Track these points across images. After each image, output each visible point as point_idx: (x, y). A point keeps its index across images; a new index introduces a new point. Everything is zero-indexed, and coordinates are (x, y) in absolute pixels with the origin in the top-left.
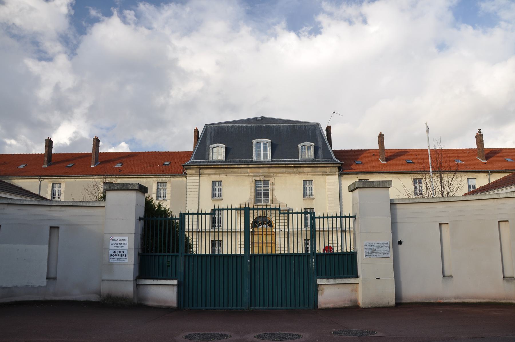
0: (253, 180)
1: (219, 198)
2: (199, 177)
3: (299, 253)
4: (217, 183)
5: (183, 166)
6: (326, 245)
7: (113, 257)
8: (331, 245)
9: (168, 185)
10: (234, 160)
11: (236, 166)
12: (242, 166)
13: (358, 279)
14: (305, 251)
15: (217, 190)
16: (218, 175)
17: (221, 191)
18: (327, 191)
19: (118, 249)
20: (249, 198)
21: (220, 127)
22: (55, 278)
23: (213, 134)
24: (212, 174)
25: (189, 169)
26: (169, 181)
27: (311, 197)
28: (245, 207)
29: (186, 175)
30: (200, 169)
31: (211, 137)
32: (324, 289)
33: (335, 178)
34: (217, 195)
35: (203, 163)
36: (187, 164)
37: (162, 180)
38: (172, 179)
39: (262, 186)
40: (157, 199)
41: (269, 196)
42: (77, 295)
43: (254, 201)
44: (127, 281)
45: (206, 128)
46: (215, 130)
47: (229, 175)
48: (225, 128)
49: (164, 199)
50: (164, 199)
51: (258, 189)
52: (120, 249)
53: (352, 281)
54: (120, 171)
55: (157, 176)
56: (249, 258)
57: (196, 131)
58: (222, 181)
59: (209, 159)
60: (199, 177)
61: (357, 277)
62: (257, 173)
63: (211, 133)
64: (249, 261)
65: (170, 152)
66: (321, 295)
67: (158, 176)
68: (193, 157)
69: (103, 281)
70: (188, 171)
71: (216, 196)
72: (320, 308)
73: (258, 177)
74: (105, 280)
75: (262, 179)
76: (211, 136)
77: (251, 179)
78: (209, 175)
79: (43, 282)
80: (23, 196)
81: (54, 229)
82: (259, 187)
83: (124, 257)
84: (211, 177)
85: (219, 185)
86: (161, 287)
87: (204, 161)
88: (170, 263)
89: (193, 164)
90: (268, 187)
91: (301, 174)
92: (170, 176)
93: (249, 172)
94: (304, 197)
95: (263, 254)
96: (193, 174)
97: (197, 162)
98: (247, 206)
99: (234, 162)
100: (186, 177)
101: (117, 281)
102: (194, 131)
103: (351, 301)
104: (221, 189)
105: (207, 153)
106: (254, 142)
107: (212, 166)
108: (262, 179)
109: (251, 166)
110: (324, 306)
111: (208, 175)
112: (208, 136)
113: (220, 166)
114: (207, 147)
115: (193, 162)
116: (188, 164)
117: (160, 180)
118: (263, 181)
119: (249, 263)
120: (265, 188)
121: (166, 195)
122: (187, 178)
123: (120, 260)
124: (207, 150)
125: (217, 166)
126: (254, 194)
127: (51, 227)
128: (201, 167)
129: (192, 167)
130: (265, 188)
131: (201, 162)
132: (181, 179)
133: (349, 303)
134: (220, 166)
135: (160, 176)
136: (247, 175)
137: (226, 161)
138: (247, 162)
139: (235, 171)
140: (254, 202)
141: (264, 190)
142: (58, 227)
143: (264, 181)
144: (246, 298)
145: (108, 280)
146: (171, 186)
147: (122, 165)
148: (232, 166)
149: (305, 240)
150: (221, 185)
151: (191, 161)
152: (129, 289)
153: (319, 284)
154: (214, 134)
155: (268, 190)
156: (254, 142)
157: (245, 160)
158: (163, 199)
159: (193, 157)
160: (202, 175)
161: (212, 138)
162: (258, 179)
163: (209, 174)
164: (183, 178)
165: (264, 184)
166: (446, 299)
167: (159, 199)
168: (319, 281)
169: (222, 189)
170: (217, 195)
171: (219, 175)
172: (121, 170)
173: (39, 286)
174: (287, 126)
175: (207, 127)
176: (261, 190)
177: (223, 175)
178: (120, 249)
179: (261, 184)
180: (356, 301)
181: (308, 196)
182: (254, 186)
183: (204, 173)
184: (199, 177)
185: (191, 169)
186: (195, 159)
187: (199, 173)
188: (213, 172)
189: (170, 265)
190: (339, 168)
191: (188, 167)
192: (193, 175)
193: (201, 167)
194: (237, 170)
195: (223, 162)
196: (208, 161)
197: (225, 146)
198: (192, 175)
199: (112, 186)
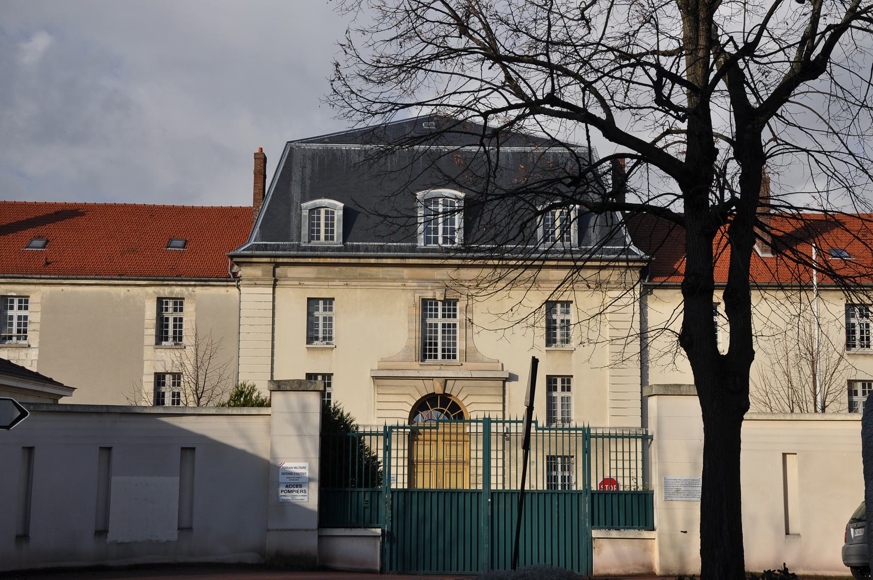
0: (417, 299)
1: (325, 342)
2: (274, 286)
3: (532, 489)
4: (321, 302)
5: (232, 257)
6: (607, 475)
7: (285, 494)
8: (613, 474)
9: (189, 308)
10: (367, 243)
11: (373, 261)
12: (389, 261)
13: (654, 532)
14: (548, 485)
15: (321, 322)
16: (323, 283)
17: (331, 325)
18: (608, 330)
19: (292, 481)
20: (404, 345)
21: (327, 150)
22: (190, 529)
23: (308, 171)
24: (310, 279)
25: (246, 266)
26: (191, 295)
27: (567, 347)
28: (484, 418)
29: (238, 281)
30: (277, 265)
31: (303, 179)
32: (602, 546)
33: (631, 299)
34: (321, 335)
35: (285, 250)
36: (240, 251)
37: (172, 293)
38: (198, 290)
39: (440, 313)
40: (157, 344)
41: (458, 341)
42: (224, 553)
43: (417, 352)
44: (307, 530)
45: (289, 153)
46: (313, 158)
47: (353, 283)
48: (342, 154)
49: (175, 345)
50: (175, 345)
51: (429, 321)
52: (296, 481)
53: (646, 534)
54: (47, 263)
55: (157, 282)
56: (490, 496)
57: (261, 159)
58: (333, 299)
59: (299, 238)
60: (274, 286)
61: (653, 529)
62: (428, 280)
63: (304, 167)
64: (490, 500)
65: (178, 207)
66: (598, 554)
67: (160, 283)
68: (256, 231)
69: (268, 530)
70: (245, 272)
71: (317, 339)
72: (596, 574)
73: (429, 291)
74: (272, 530)
75: (440, 296)
76: (303, 175)
77: (410, 294)
78: (301, 282)
79: (173, 535)
80: (43, 384)
81: (188, 451)
82: (431, 316)
83: (302, 494)
84: (307, 287)
85: (325, 309)
86: (355, 539)
87: (286, 245)
88: (369, 503)
89: (258, 253)
90: (455, 316)
91: (541, 285)
92: (193, 283)
93: (406, 277)
94: (547, 346)
95: (530, 490)
96: (258, 279)
97: (269, 247)
98: (487, 416)
99: (366, 249)
100: (238, 287)
101: (292, 530)
102: (255, 159)
103: (643, 565)
104: (331, 319)
105: (294, 221)
106: (420, 195)
107: (310, 260)
108: (439, 296)
109: (411, 261)
110: (602, 572)
111: (297, 283)
112: (296, 176)
113: (329, 260)
114: (295, 204)
115: (258, 247)
116: (246, 252)
117: (165, 291)
118: (441, 301)
119: (490, 504)
120: (448, 321)
121: (181, 332)
122: (241, 288)
123: (297, 498)
124: (293, 214)
125: (322, 260)
126: (419, 334)
127: (182, 448)
128: (281, 260)
129: (255, 260)
130: (448, 321)
131: (277, 248)
132: (222, 290)
133: (641, 568)
134: (329, 260)
135: (166, 283)
136: (400, 284)
137: (345, 246)
138: (401, 249)
139: (367, 272)
140: (417, 356)
141: (444, 325)
142: (194, 449)
143: (446, 302)
144: (484, 556)
145: (277, 530)
146: (196, 309)
147: (46, 244)
148: (362, 261)
149: (547, 456)
150: (331, 309)
151: (252, 242)
152: (309, 543)
153: (594, 538)
154: (313, 170)
155: (455, 325)
156: (420, 195)
157: (395, 244)
158: (173, 344)
159: (256, 231)
160: (282, 283)
161: (308, 182)
162: (429, 295)
163: (300, 279)
164: (228, 289)
165: (444, 310)
166: (804, 570)
167: (164, 343)
168: (595, 533)
169: (334, 319)
170: (321, 335)
171: (326, 283)
172: (49, 260)
173: (168, 541)
174: (508, 153)
175: (292, 149)
176: (436, 325)
177: (337, 283)
178: (296, 481)
179: (436, 310)
180: (650, 566)
181: (558, 343)
182: (418, 313)
183: (286, 277)
184: (274, 288)
185: (250, 266)
186: (263, 237)
187: (274, 275)
188: (312, 276)
189: (369, 505)
190: (640, 272)
191: (245, 261)
192: (258, 282)
193: (281, 260)
194: (374, 270)
195: (339, 249)
196: (299, 245)
197: (342, 205)
198: (254, 282)
199: (283, 384)
